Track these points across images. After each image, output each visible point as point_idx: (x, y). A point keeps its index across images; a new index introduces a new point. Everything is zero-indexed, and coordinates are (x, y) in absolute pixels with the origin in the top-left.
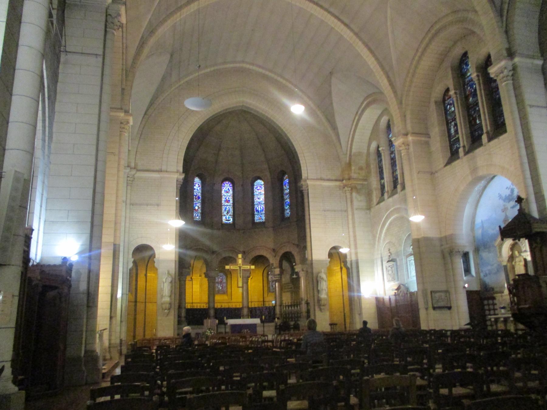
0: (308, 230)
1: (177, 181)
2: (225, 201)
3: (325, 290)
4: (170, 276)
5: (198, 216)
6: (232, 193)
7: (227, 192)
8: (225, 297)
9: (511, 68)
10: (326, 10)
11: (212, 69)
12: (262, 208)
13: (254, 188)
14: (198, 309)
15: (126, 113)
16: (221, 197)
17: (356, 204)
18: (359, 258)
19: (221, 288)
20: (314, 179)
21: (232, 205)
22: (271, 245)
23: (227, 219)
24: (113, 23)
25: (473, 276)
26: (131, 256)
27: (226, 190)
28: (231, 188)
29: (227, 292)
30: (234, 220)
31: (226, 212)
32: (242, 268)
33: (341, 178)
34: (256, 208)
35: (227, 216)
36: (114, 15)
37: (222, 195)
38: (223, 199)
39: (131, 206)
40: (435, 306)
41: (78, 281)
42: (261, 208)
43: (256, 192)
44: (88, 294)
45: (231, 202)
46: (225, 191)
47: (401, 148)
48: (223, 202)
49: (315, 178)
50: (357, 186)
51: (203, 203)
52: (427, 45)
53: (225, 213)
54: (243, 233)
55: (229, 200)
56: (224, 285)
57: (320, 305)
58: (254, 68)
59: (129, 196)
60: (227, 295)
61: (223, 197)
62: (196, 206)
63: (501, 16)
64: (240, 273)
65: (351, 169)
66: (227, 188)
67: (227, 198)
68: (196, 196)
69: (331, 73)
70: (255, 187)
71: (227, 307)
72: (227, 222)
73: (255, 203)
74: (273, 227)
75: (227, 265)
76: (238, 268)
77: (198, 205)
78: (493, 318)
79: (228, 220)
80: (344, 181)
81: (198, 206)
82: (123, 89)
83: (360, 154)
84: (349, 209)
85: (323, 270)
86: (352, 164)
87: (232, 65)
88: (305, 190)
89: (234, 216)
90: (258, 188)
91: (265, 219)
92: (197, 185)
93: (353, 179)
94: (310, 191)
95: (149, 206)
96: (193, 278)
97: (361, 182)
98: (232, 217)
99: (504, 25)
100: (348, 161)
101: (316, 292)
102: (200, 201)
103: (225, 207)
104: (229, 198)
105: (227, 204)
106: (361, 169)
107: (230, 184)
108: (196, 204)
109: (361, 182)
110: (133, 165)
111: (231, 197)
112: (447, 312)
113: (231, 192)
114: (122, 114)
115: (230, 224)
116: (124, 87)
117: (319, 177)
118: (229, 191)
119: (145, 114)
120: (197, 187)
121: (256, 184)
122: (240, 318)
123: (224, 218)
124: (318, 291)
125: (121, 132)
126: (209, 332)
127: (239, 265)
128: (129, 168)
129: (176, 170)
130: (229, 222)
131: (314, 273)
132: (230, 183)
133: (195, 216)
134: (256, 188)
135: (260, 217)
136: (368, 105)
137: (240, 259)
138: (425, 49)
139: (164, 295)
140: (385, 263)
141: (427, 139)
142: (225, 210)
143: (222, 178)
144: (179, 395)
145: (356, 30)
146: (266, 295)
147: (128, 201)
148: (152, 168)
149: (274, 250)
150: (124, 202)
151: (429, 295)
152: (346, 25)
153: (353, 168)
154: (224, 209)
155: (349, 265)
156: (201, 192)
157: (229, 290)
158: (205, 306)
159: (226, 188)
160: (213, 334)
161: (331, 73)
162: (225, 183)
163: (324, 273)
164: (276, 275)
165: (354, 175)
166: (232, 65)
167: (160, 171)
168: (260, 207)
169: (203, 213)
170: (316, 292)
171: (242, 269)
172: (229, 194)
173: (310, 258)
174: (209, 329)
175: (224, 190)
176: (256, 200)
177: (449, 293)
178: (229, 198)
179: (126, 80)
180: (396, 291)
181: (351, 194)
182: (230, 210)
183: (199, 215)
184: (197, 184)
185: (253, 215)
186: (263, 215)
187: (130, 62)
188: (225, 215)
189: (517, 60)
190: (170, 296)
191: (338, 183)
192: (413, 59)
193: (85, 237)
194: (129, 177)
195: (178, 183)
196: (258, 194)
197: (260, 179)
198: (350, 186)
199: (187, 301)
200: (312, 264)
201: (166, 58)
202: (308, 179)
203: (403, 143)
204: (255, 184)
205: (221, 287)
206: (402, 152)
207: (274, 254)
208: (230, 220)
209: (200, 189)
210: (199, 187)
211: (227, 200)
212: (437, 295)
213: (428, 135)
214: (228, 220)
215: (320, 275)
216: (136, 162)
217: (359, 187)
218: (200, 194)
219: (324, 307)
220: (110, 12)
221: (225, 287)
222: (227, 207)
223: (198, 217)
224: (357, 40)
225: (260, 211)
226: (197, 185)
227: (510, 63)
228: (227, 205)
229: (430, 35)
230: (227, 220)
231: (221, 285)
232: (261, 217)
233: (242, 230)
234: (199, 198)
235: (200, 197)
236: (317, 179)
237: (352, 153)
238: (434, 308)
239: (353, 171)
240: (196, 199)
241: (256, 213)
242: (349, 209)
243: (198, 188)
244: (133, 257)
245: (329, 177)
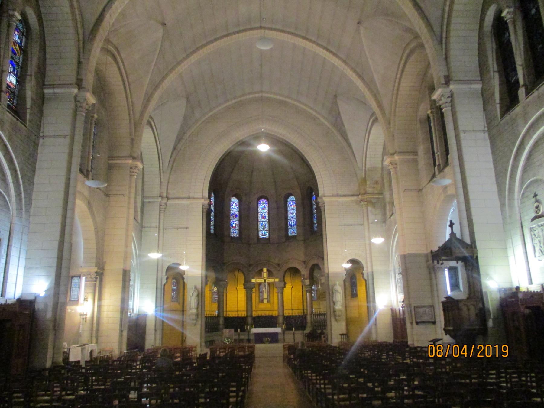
0: (325, 245)
1: (203, 206)
2: (261, 217)
3: (340, 302)
4: (196, 291)
5: (235, 232)
6: (268, 209)
7: (263, 209)
9: (449, 95)
10: (314, 42)
11: (233, 101)
14: (231, 317)
15: (135, 160)
16: (258, 213)
17: (371, 217)
18: (374, 270)
20: (331, 196)
21: (268, 221)
22: (302, 257)
23: (264, 234)
24: (81, 107)
25: (461, 291)
26: (164, 273)
27: (262, 207)
31: (262, 228)
32: (267, 281)
33: (358, 193)
34: (290, 223)
35: (264, 231)
36: (81, 100)
37: (259, 212)
38: (260, 216)
39: (165, 230)
40: (418, 320)
41: (45, 311)
42: (293, 223)
44: (55, 320)
45: (267, 218)
46: (261, 207)
47: (390, 167)
48: (260, 218)
49: (332, 194)
50: (372, 200)
51: (240, 221)
52: (404, 66)
53: (261, 229)
57: (335, 316)
58: (272, 96)
59: (162, 221)
60: (270, 304)
61: (260, 213)
62: (234, 224)
63: (441, 43)
64: (265, 286)
65: (366, 184)
66: (263, 205)
67: (263, 214)
68: (233, 214)
69: (335, 96)
70: (288, 203)
71: (270, 314)
72: (263, 236)
73: (288, 218)
74: (304, 241)
75: (254, 278)
76: (263, 281)
80: (360, 196)
81: (236, 224)
82: (133, 140)
83: (373, 169)
84: (366, 223)
85: (337, 283)
86: (367, 178)
87: (251, 96)
88: (322, 207)
89: (269, 231)
90: (292, 204)
91: (297, 234)
92: (234, 205)
93: (368, 193)
94: (326, 207)
95: (179, 230)
96: (237, 288)
97: (377, 196)
99: (444, 52)
100: (364, 176)
101: (332, 304)
102: (237, 218)
103: (262, 223)
104: (265, 215)
105: (263, 220)
106: (376, 183)
107: (265, 202)
108: (233, 222)
109: (377, 196)
110: (164, 195)
111: (267, 213)
112: (432, 326)
113: (267, 209)
114: (131, 161)
115: (265, 239)
116: (133, 137)
117: (336, 193)
118: (265, 208)
119: (174, 148)
120: (235, 207)
123: (260, 233)
124: (334, 303)
125: (131, 175)
126: (227, 340)
127: (264, 279)
128: (161, 198)
129: (201, 197)
130: (265, 236)
131: (330, 285)
132: (265, 200)
133: (233, 233)
134: (289, 204)
135: (293, 231)
136: (372, 124)
137: (265, 272)
138: (403, 71)
139: (191, 307)
140: (397, 275)
141: (415, 157)
142: (261, 226)
143: (257, 196)
144: (491, 386)
145: (344, 57)
147: (161, 227)
148: (182, 196)
149: (304, 262)
150: (157, 227)
151: (413, 309)
152: (334, 54)
153: (368, 183)
154: (260, 225)
155: (365, 277)
156: (238, 210)
158: (243, 314)
159: (262, 205)
160: (230, 342)
161: (335, 96)
162: (261, 200)
163: (339, 285)
164: (307, 286)
165: (369, 190)
166: (251, 96)
167: (189, 198)
168: (293, 222)
169: (240, 231)
170: (332, 304)
171: (267, 282)
172: (265, 211)
173: (326, 271)
174: (227, 338)
175: (260, 207)
176: (290, 216)
177: (434, 307)
178: (265, 215)
179: (135, 131)
180: (403, 303)
181: (367, 207)
182: (266, 226)
183: (237, 231)
184: (234, 204)
185: (287, 230)
186: (295, 229)
187: (138, 115)
189: (452, 87)
190: (197, 308)
191: (354, 198)
192: (395, 82)
193: (53, 277)
194: (161, 205)
195: (204, 207)
197: (293, 195)
198: (366, 200)
200: (328, 277)
201: (183, 103)
202: (324, 196)
203: (391, 163)
204: (289, 200)
206: (391, 170)
207: (304, 266)
208: (266, 235)
209: (237, 208)
210: (236, 206)
211: (263, 216)
212: (421, 310)
213: (415, 153)
215: (335, 287)
216: (168, 191)
217: (374, 201)
218: (237, 213)
219: (339, 318)
220: (78, 99)
222: (263, 223)
223: (235, 234)
224: (346, 67)
226: (234, 205)
227: (447, 90)
228: (263, 221)
229: (404, 58)
230: (263, 235)
232: (294, 231)
233: (277, 244)
234: (236, 216)
235: (238, 215)
236: (333, 196)
237: (367, 168)
238: (417, 323)
239: (368, 186)
240: (233, 217)
241: (289, 227)
242: (366, 223)
243: (236, 207)
244: (166, 275)
245: (345, 193)
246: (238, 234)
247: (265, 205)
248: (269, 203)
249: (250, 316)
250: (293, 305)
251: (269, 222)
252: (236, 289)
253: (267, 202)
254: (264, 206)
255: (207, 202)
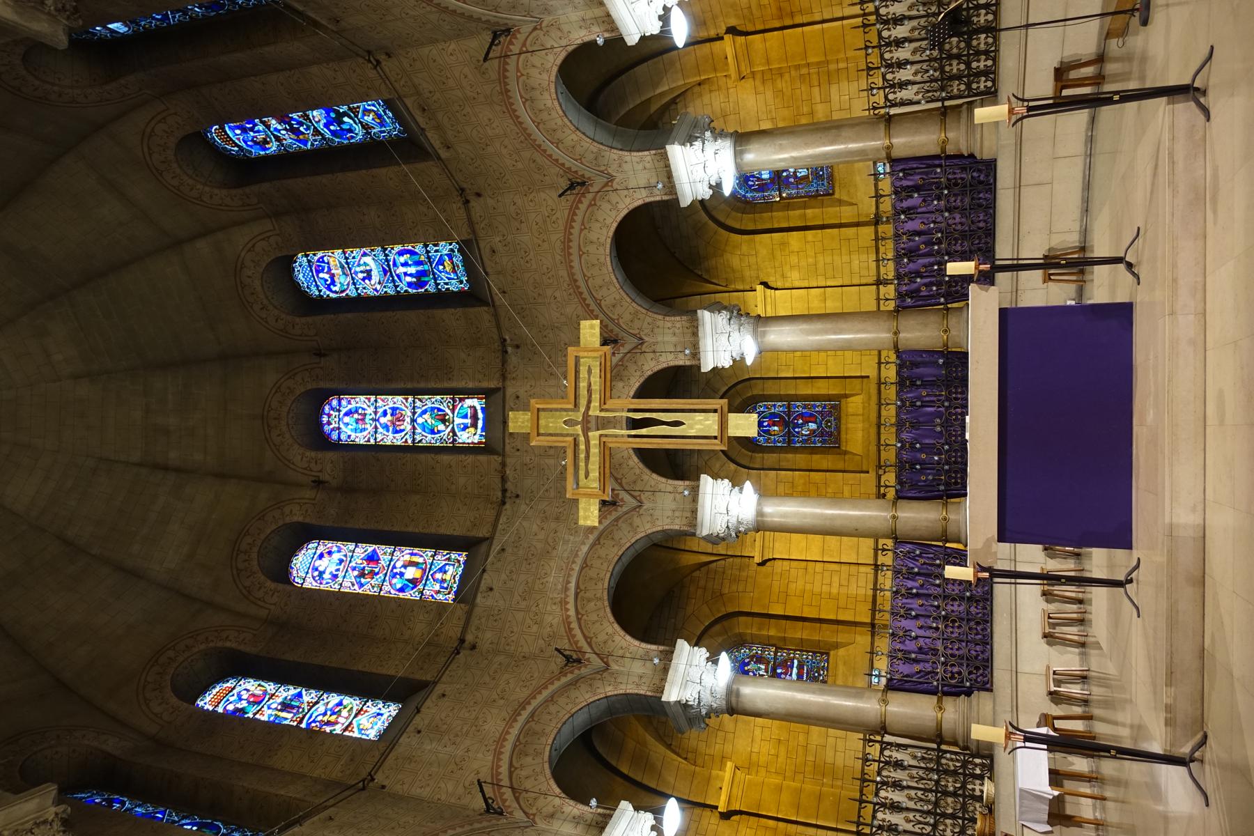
8: (855, 405)
12: (402, 259)
13: (333, 295)
16: (378, 448)
19: (813, 426)
21: (410, 399)
23: (468, 421)
28: (344, 403)
29: (829, 398)
30: (471, 393)
31: (441, 427)
32: (595, 412)
34: (410, 284)
35: (458, 421)
37: (372, 442)
38: (390, 439)
42: (405, 264)
43: (343, 286)
54: (518, 347)
55: (394, 409)
56: (799, 407)
62: (402, 574)
66: (347, 419)
67: (383, 420)
72: (480, 424)
73: (391, 292)
76: (594, 435)
77: (399, 564)
78: (950, 780)
79: (475, 417)
92: (322, 564)
96: (758, 560)
98: (461, 400)
102: (384, 551)
104: (385, 413)
111: (380, 403)
113: (360, 401)
121: (313, 288)
122: (962, 358)
123: (466, 437)
130: (480, 415)
132: (327, 409)
137: (723, 425)
142: (432, 432)
146: (847, 214)
157: (822, 388)
162: (327, 428)
168: (401, 270)
176: (374, 286)
178: (385, 413)
183: (440, 560)
185: (444, 299)
188: (453, 430)
196: (349, 279)
199: (894, 474)
205: (936, 232)
208: (474, 408)
214: (475, 417)
221: (805, 407)
225: (420, 268)
228: (413, 421)
230: (475, 425)
231: (797, 426)
234: (372, 558)
235: (370, 548)
241: (430, 288)
243: (336, 556)
246: (347, 590)
247: (344, 411)
248: (339, 393)
249: (885, 702)
250: (855, 281)
251: (415, 392)
252: (763, 563)
253: (335, 403)
254: (347, 414)
255: (848, 436)
